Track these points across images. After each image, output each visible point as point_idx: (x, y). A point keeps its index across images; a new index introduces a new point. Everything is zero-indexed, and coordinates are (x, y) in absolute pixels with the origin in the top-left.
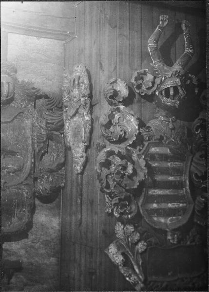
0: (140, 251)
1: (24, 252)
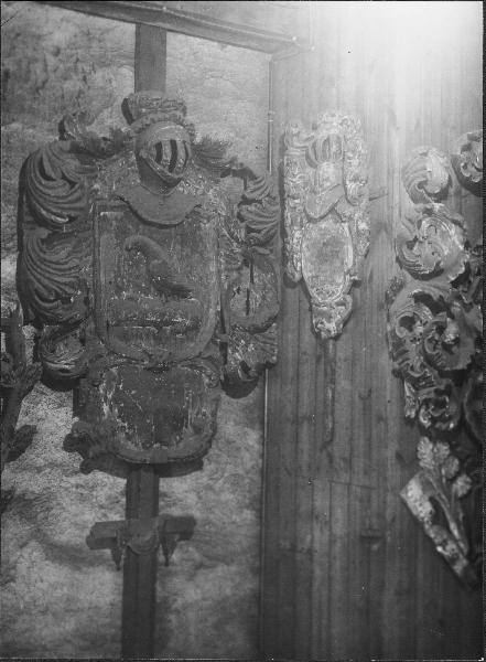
0: (460, 493)
1: (195, 499)
